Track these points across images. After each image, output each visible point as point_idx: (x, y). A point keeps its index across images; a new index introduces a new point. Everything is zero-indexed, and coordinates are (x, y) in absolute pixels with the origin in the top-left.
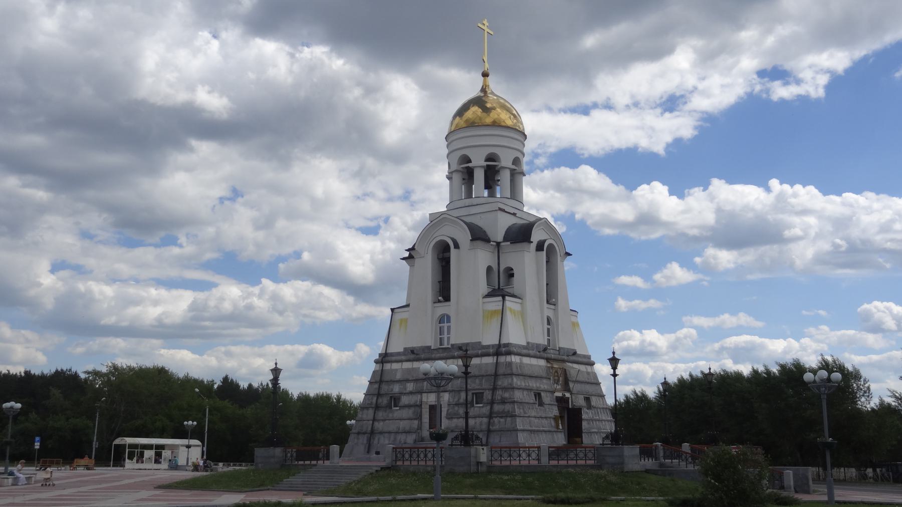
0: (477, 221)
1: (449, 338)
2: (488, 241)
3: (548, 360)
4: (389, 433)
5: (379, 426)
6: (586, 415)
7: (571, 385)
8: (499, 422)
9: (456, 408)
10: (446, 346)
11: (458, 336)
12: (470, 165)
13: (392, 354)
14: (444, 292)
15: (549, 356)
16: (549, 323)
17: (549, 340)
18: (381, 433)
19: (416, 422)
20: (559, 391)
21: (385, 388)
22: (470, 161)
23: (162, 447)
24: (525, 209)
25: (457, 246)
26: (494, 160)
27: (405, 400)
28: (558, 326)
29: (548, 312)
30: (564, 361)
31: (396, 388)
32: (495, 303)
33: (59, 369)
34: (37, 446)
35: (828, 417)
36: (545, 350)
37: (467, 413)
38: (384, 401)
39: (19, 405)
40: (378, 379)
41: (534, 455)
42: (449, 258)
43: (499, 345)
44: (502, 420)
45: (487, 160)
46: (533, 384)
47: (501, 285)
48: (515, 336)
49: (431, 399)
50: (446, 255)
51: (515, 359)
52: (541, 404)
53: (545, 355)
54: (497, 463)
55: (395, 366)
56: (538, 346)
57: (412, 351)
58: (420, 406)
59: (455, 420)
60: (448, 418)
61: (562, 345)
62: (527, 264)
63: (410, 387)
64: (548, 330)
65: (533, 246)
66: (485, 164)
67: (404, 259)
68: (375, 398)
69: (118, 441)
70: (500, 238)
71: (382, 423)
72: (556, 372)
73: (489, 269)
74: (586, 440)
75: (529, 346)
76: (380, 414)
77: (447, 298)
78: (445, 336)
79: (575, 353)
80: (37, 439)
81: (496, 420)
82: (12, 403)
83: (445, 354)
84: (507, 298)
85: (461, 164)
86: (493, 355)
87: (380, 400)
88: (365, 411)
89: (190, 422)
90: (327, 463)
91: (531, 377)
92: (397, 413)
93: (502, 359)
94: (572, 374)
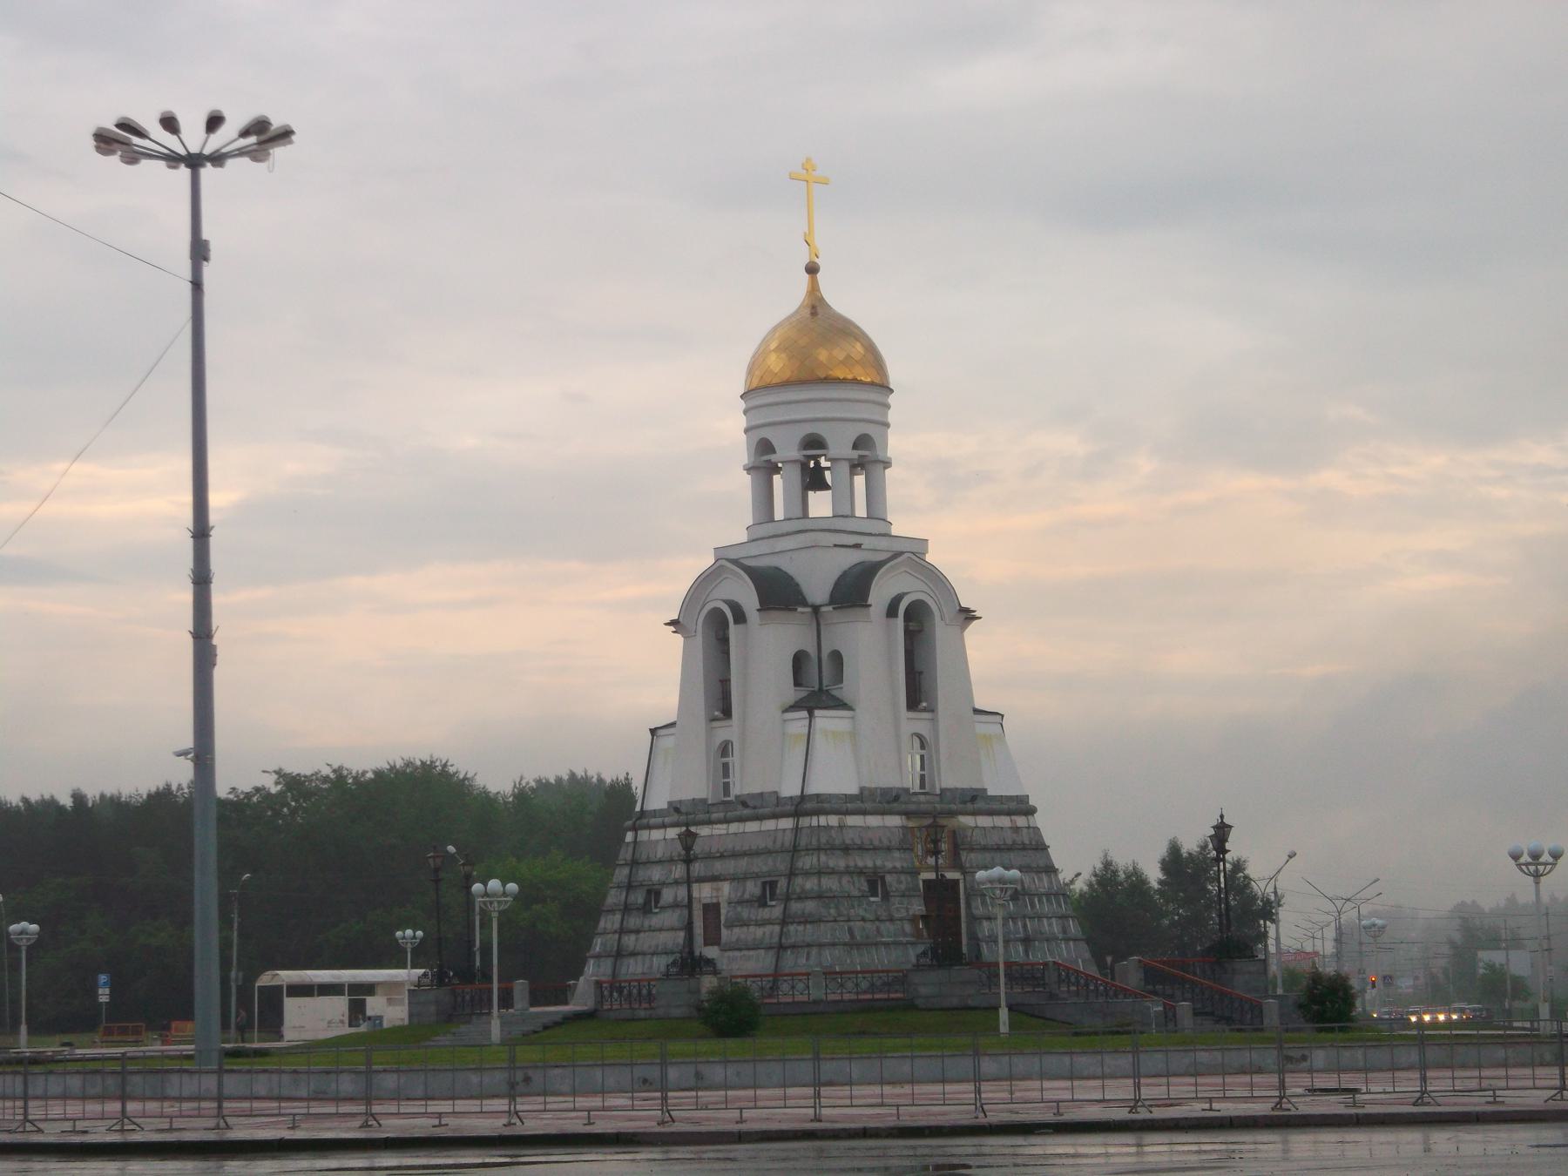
2: (804, 603)
3: (907, 814)
5: (630, 941)
7: (964, 855)
12: (773, 458)
13: (655, 813)
17: (922, 777)
18: (633, 954)
22: (774, 451)
23: (369, 989)
25: (740, 617)
27: (668, 895)
28: (938, 751)
29: (916, 723)
31: (656, 874)
33: (580, 773)
34: (104, 995)
38: (639, 898)
39: (34, 927)
43: (803, 798)
44: (801, 928)
46: (866, 861)
47: (825, 682)
55: (656, 835)
58: (689, 905)
59: (736, 930)
61: (944, 785)
62: (869, 647)
69: (266, 979)
71: (633, 937)
73: (799, 660)
77: (727, 713)
80: (103, 978)
81: (792, 928)
82: (24, 924)
84: (817, 713)
87: (632, 898)
93: (805, 822)
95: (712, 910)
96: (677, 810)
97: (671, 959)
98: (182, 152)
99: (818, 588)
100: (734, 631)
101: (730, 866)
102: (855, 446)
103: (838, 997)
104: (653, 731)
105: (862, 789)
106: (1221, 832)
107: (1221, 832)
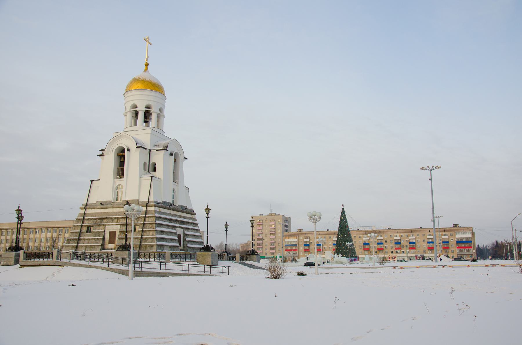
11: (125, 197)
14: (120, 172)
16: (174, 192)
22: (137, 107)
24: (165, 134)
25: (128, 150)
26: (149, 108)
37: (18, 233)
42: (124, 156)
45: (146, 107)
64: (173, 195)
67: (99, 156)
75: (164, 203)
78: (119, 196)
79: (186, 208)
89: (349, 243)
100: (126, 153)
104: (92, 181)
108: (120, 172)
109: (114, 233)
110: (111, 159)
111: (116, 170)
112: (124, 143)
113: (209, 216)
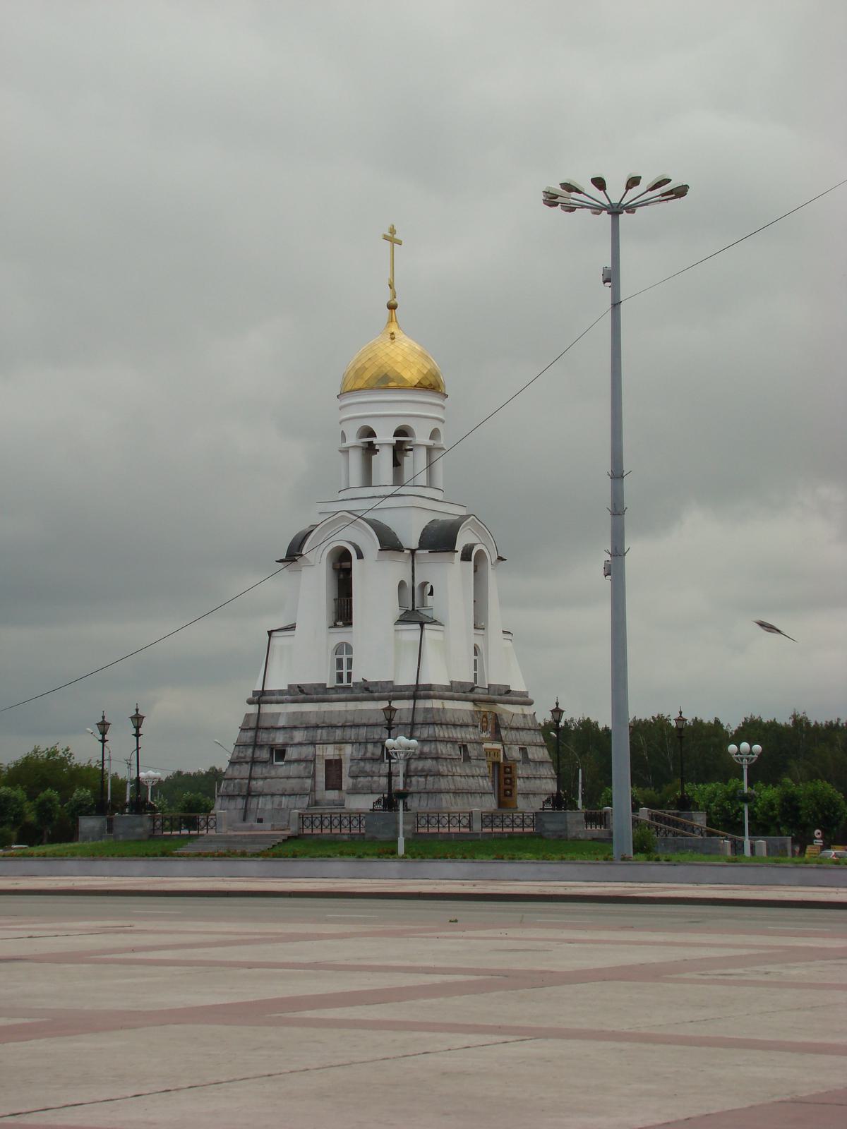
0: (386, 519)
1: (349, 675)
3: (474, 701)
4: (273, 795)
5: (257, 785)
6: (521, 771)
7: (503, 733)
8: (418, 782)
9: (362, 764)
10: (345, 683)
13: (272, 693)
14: (343, 613)
15: (476, 696)
16: (476, 654)
17: (475, 675)
18: (260, 795)
19: (309, 782)
20: (488, 740)
21: (264, 737)
25: (360, 556)
27: (292, 753)
30: (494, 702)
31: (280, 738)
32: (410, 633)
35: (111, 784)
36: (472, 690)
40: (253, 724)
41: (465, 822)
44: (422, 779)
46: (457, 734)
48: (436, 675)
49: (330, 752)
50: (346, 565)
51: (436, 704)
52: (467, 758)
53: (472, 696)
54: (422, 830)
56: (462, 684)
57: (300, 689)
58: (313, 761)
60: (352, 777)
63: (299, 736)
64: (475, 661)
65: (458, 556)
66: (393, 440)
68: (250, 751)
70: (415, 545)
72: (485, 716)
73: (402, 585)
74: (521, 803)
76: (259, 771)
79: (508, 692)
83: (343, 696)
84: (426, 626)
85: (361, 437)
86: (408, 698)
88: (237, 767)
90: (212, 832)
91: (455, 725)
92: (281, 769)
93: (422, 704)
94: (506, 719)
95: (334, 766)
96: (302, 691)
97: (376, 797)
98: (607, 203)
99: (411, 538)
100: (356, 563)
101: (351, 734)
102: (431, 438)
103: (436, 830)
104: (270, 633)
105: (290, 686)
106: (775, 720)
107: (775, 720)
108: (343, 613)
109: (339, 763)
110: (315, 578)
111: (333, 603)
112: (345, 537)
113: (141, 731)
